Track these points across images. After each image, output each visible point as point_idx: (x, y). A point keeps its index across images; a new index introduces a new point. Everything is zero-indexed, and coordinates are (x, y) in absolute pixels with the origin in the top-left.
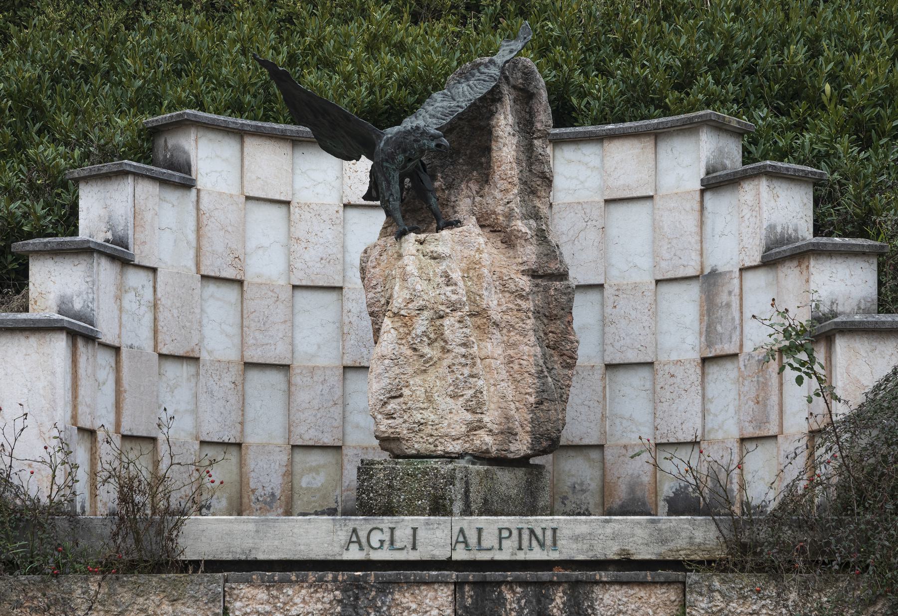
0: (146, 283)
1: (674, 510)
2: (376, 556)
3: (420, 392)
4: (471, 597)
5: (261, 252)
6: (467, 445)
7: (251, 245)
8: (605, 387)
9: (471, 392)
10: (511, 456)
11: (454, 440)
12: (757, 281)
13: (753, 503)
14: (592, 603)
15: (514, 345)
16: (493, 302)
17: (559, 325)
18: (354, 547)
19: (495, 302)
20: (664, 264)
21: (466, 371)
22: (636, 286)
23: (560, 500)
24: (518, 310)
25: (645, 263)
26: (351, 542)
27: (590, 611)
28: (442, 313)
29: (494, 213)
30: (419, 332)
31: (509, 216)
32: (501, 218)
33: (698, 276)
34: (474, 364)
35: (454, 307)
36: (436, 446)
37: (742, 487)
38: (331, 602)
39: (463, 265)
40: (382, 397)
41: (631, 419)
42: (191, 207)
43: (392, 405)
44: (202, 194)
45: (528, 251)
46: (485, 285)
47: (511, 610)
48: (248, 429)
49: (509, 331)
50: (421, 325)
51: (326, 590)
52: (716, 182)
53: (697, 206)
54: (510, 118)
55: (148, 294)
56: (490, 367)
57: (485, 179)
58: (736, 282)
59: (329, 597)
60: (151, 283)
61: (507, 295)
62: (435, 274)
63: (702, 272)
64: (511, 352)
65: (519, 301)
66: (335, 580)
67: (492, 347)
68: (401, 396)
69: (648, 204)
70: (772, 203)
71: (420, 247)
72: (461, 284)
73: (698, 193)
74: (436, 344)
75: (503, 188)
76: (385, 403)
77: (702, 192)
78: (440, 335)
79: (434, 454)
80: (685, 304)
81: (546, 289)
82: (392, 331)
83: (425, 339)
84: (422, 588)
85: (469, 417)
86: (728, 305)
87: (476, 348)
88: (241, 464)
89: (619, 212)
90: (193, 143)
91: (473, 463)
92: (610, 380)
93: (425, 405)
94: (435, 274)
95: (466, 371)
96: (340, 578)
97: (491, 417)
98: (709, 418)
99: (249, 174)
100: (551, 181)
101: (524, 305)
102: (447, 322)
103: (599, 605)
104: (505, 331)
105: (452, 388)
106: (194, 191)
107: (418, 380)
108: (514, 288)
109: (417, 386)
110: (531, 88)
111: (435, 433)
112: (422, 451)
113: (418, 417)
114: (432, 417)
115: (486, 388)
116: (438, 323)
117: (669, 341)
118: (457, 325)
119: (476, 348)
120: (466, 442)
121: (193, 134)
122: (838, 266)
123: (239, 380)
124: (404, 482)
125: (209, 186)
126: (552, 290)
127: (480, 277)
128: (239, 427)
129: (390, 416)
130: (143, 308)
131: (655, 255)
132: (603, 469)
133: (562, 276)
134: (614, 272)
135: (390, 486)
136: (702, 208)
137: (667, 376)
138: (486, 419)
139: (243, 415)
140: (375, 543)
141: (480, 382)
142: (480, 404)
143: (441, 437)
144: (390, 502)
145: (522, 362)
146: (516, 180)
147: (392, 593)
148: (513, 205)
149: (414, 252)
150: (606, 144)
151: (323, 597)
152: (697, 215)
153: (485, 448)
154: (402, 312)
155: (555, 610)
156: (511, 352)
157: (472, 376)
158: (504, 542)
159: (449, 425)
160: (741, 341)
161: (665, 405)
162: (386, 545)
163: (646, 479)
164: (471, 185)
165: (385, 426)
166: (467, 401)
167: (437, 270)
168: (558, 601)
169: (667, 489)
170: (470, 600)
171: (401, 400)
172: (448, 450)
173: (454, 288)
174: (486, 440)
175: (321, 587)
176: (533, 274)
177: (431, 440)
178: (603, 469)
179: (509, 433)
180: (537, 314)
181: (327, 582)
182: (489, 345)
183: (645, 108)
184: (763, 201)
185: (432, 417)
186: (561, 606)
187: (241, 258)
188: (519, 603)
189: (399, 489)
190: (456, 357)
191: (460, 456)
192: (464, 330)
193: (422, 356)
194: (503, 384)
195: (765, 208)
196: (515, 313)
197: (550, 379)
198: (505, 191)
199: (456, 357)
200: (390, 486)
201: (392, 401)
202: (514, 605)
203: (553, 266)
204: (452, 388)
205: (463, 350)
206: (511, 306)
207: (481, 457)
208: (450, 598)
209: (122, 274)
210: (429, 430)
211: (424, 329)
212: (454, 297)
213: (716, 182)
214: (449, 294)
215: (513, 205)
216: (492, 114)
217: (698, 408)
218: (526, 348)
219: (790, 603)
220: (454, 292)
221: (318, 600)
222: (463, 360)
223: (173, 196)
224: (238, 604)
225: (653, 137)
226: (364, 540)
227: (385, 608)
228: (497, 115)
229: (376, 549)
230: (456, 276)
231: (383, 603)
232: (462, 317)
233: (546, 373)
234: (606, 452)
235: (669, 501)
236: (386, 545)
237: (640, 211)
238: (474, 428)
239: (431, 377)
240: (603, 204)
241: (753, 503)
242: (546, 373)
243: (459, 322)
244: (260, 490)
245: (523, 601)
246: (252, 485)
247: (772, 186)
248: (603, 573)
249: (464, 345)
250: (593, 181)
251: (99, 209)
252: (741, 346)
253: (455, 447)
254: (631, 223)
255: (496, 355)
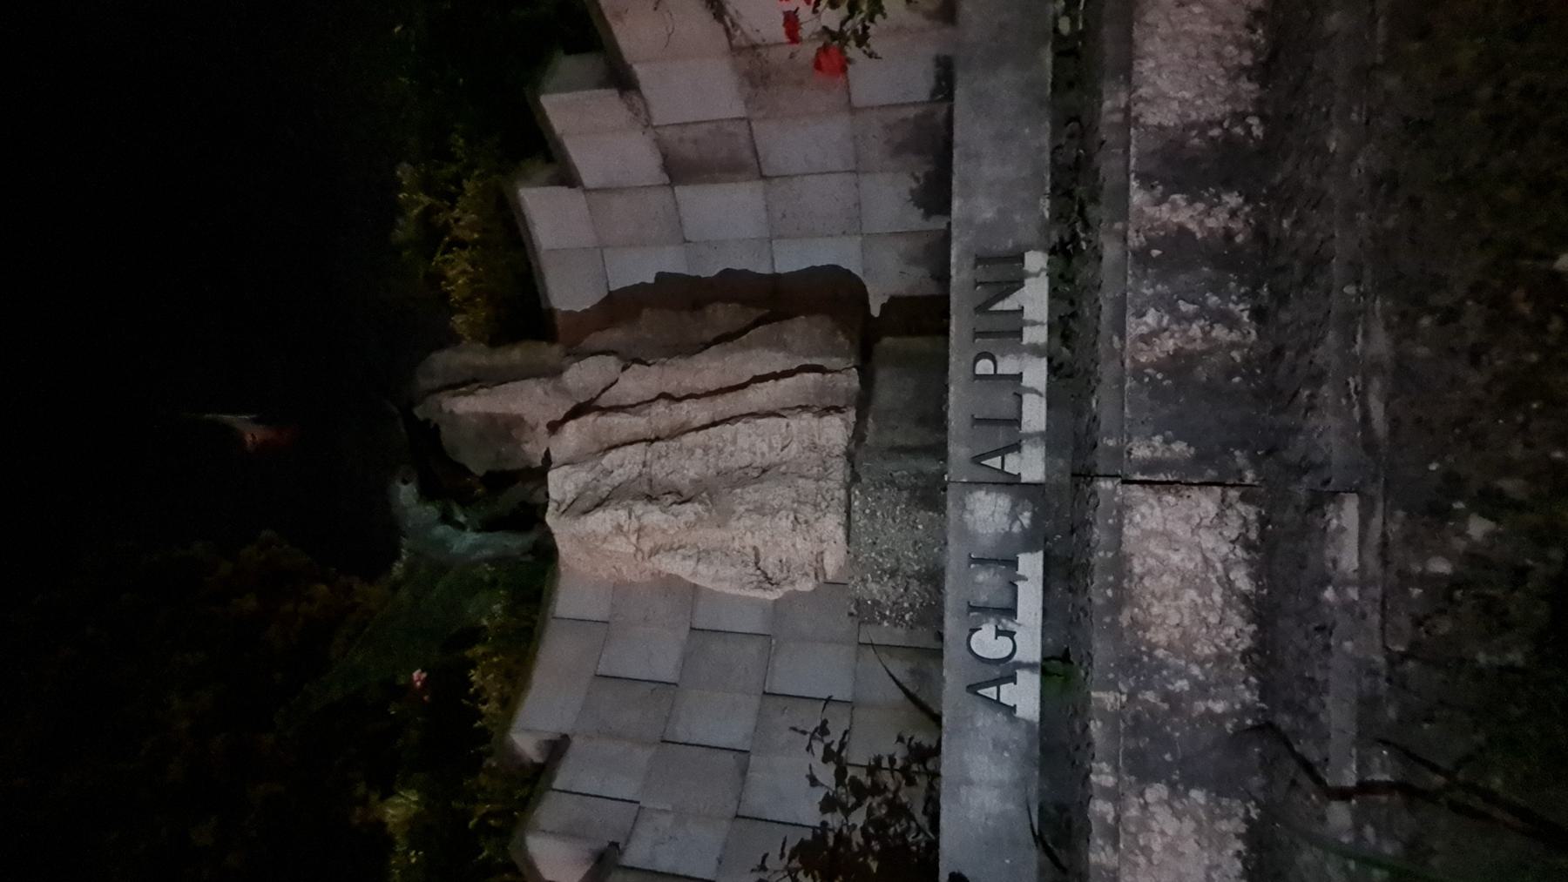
1: (944, 208)
4: (1167, 442)
14: (1192, 126)
27: (1215, 132)
38: (1178, 815)
51: (1144, 826)
59: (1164, 820)
66: (1114, 796)
86: (695, 141)
96: (1109, 781)
103: (1198, 109)
124: (887, 551)
135: (893, 574)
144: (917, 576)
147: (1153, 647)
151: (1163, 833)
163: (903, 244)
169: (915, 219)
175: (1135, 836)
181: (1117, 819)
186: (1200, 206)
188: (1190, 319)
189: (898, 560)
200: (893, 574)
208: (1170, 499)
209: (1248, 8)
227: (1195, 670)
231: (1180, 673)
235: (928, 214)
245: (1184, 307)
248: (1108, 104)
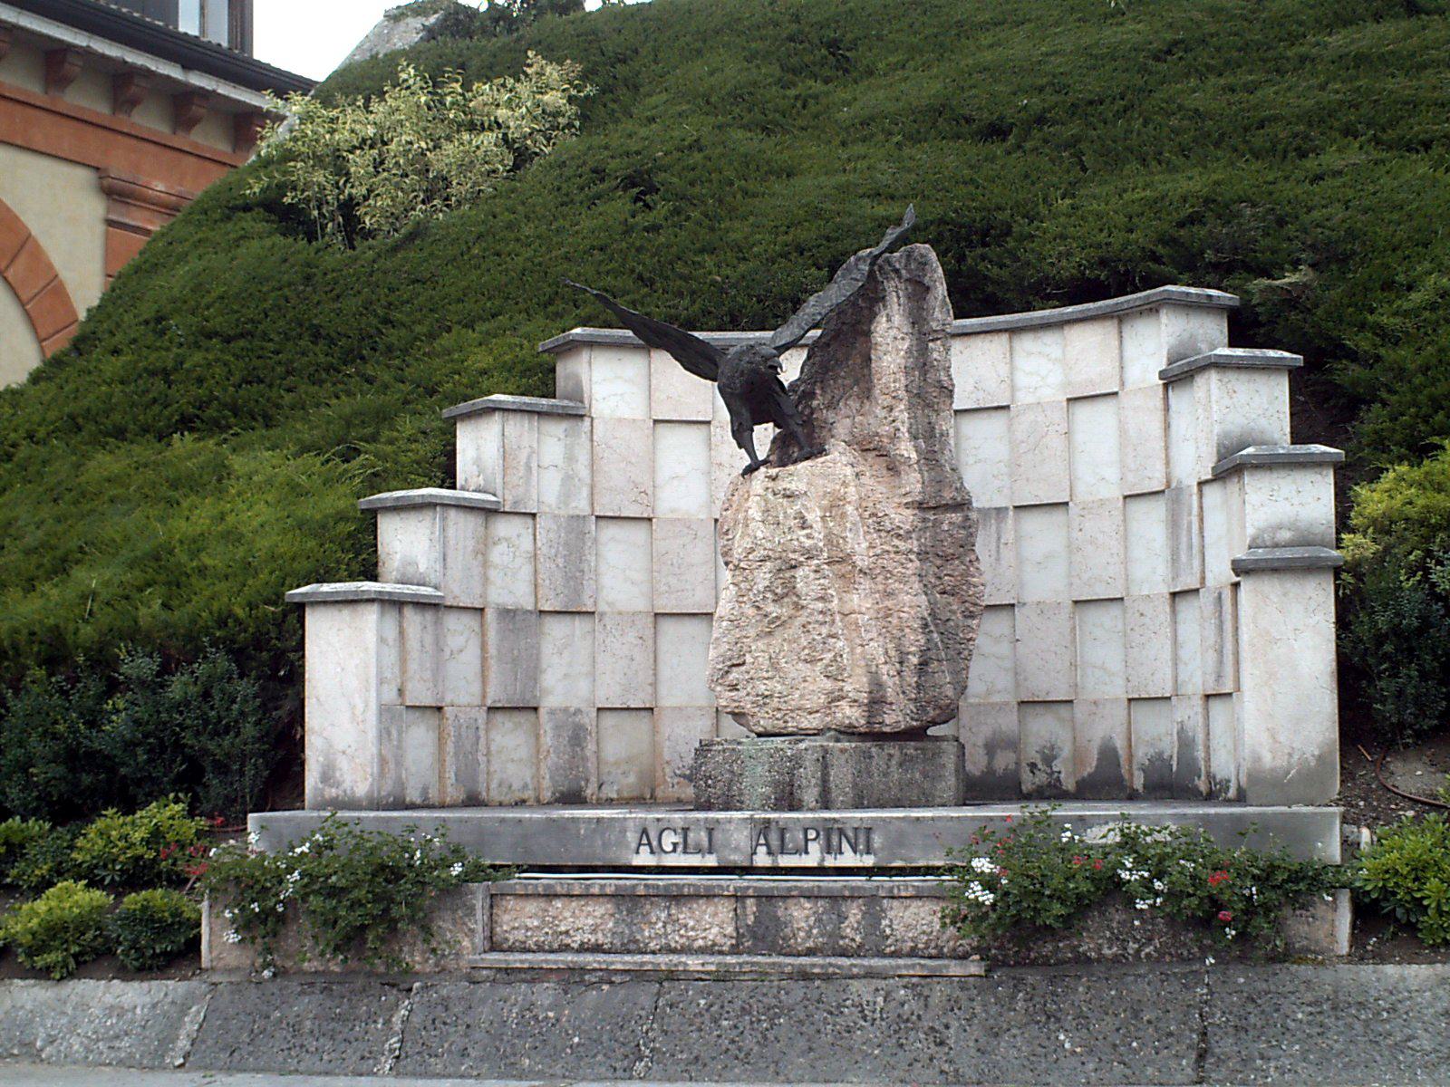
0: (523, 531)
2: (670, 861)
3: (763, 660)
5: (675, 482)
6: (828, 719)
7: (663, 474)
8: (1074, 628)
9: (830, 656)
10: (887, 729)
11: (810, 713)
12: (1213, 494)
13: (1218, 778)
15: (889, 594)
16: (860, 546)
17: (956, 567)
18: (645, 849)
19: (864, 545)
20: (1130, 477)
21: (824, 631)
22: (1102, 503)
23: (1028, 769)
24: (896, 553)
25: (1112, 473)
26: (640, 844)
28: (793, 562)
29: (877, 434)
30: (761, 587)
31: (894, 437)
32: (885, 440)
33: (1163, 492)
34: (833, 622)
35: (810, 554)
36: (786, 722)
37: (1208, 760)
38: (602, 917)
39: (825, 502)
40: (720, 666)
41: (1103, 668)
42: (584, 439)
43: (735, 675)
44: (596, 422)
45: (912, 480)
46: (848, 525)
47: (799, 929)
48: (663, 690)
49: (887, 578)
50: (763, 578)
52: (1178, 376)
53: (1159, 404)
54: (897, 319)
55: (526, 544)
56: (856, 624)
57: (867, 395)
58: (1195, 498)
60: (530, 530)
61: (883, 534)
62: (786, 516)
63: (1168, 486)
64: (889, 603)
65: (896, 542)
67: (861, 600)
68: (744, 663)
69: (1111, 402)
70: (1227, 401)
71: (771, 484)
72: (818, 526)
73: (1161, 389)
74: (786, 600)
75: (885, 404)
76: (727, 672)
77: (1166, 386)
78: (790, 589)
79: (784, 731)
80: (1151, 522)
81: (937, 524)
82: (731, 587)
83: (769, 595)
84: (701, 902)
85: (829, 685)
87: (836, 601)
88: (655, 731)
89: (1082, 411)
90: (585, 365)
91: (838, 740)
92: (1081, 620)
93: (770, 674)
94: (786, 516)
95: (824, 631)
97: (856, 685)
98: (1181, 667)
99: (657, 394)
100: (951, 391)
101: (902, 545)
102: (800, 573)
104: (880, 578)
105: (806, 651)
106: (587, 421)
107: (761, 644)
108: (888, 526)
109: (758, 653)
110: (926, 280)
111: (783, 707)
112: (769, 728)
113: (762, 688)
114: (779, 687)
115: (847, 650)
116: (788, 575)
117: (1139, 572)
118: (812, 575)
119: (836, 601)
120: (827, 715)
121: (585, 355)
122: (1280, 481)
123: (649, 633)
125: (607, 412)
126: (947, 523)
127: (843, 515)
128: (650, 690)
129: (734, 688)
130: (519, 561)
131: (1123, 465)
132: (1074, 729)
133: (962, 505)
134: (1081, 488)
136: (1167, 408)
137: (1137, 615)
138: (848, 687)
139: (655, 675)
140: (669, 848)
141: (840, 644)
142: (842, 669)
143: (792, 711)
145: (902, 615)
146: (902, 393)
148: (898, 424)
149: (761, 492)
150: (1067, 329)
152: (1160, 415)
153: (847, 722)
154: (742, 565)
155: (848, 930)
156: (889, 603)
157: (832, 636)
158: (810, 843)
159: (802, 696)
160: (1203, 572)
161: (1136, 649)
162: (680, 848)
164: (850, 402)
165: (725, 699)
166: (827, 666)
167: (789, 511)
168: (852, 919)
170: (752, 917)
171: (743, 668)
172: (802, 726)
173: (808, 531)
174: (850, 714)
176: (920, 506)
177: (779, 716)
178: (1074, 729)
179: (876, 702)
180: (922, 555)
182: (855, 597)
183: (1103, 284)
184: (1214, 398)
185: (779, 687)
187: (649, 492)
190: (811, 614)
191: (819, 732)
192: (822, 581)
193: (766, 616)
194: (872, 644)
195: (1215, 408)
196: (892, 555)
197: (935, 635)
198: (889, 411)
199: (811, 614)
201: (734, 669)
202: (803, 924)
203: (948, 495)
204: (806, 651)
205: (820, 605)
206: (886, 547)
207: (848, 732)
210: (775, 703)
211: (767, 583)
212: (808, 543)
213: (1178, 376)
214: (802, 539)
215: (898, 424)
216: (872, 316)
217: (1166, 654)
218: (907, 598)
219: (1114, 925)
220: (809, 537)
221: (589, 914)
222: (820, 618)
223: (556, 429)
224: (506, 918)
225: (1116, 321)
226: (655, 843)
228: (878, 318)
229: (666, 852)
230: (813, 517)
232: (818, 566)
233: (932, 628)
234: (1076, 710)
236: (680, 848)
237: (1104, 409)
238: (835, 698)
239: (776, 641)
240: (1065, 404)
241: (1218, 778)
242: (932, 628)
243: (816, 571)
244: (678, 760)
246: (667, 758)
247: (1226, 380)
249: (822, 599)
250: (1056, 377)
251: (479, 447)
252: (1203, 579)
253: (813, 722)
254: (1096, 424)
255: (864, 610)
